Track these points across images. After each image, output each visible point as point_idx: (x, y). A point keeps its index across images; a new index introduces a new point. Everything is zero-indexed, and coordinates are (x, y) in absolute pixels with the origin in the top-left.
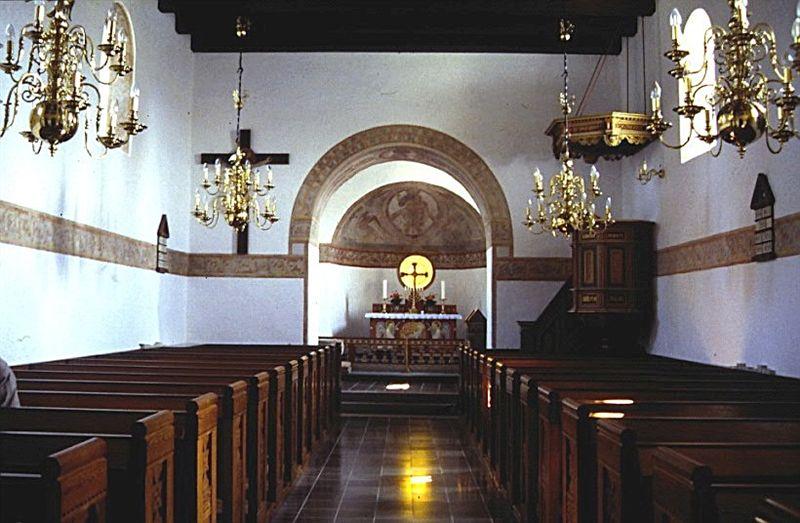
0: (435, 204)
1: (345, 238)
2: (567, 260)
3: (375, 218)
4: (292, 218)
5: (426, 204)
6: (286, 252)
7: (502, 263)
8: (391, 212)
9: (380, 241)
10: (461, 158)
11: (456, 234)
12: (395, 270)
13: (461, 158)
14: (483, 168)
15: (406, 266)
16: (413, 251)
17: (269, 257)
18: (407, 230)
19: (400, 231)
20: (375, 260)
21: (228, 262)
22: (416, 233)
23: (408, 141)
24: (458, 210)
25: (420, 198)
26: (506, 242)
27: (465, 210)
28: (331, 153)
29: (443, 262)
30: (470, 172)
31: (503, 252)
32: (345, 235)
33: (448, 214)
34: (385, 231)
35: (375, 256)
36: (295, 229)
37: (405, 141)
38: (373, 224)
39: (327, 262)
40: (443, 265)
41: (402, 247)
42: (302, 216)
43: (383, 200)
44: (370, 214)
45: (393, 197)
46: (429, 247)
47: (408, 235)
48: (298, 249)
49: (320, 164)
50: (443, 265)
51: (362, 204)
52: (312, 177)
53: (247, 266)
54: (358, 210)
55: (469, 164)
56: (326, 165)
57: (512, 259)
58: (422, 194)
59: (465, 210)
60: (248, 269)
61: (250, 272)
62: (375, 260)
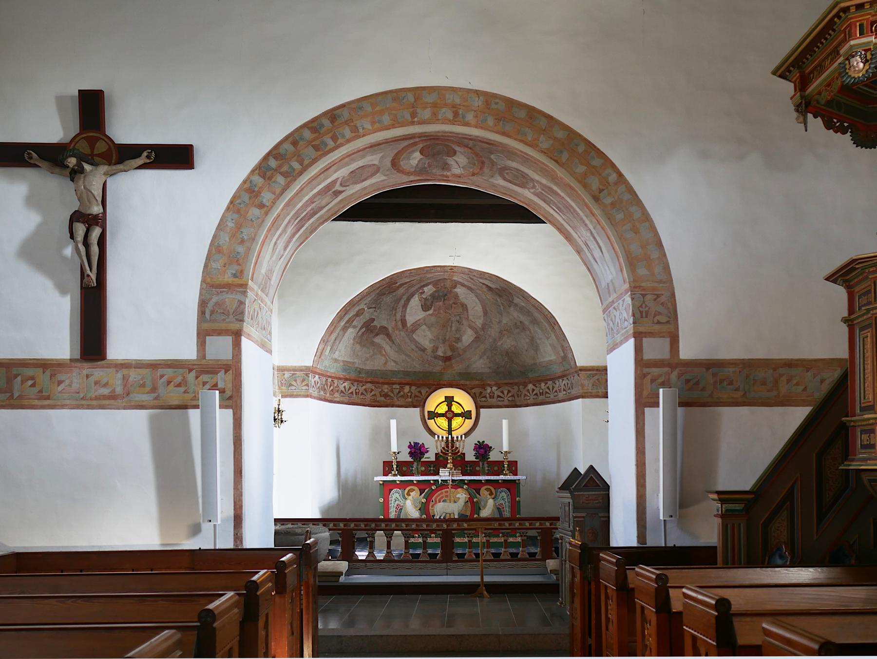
0: (479, 308)
1: (336, 360)
2: (679, 357)
3: (384, 330)
4: (204, 281)
5: (464, 307)
6: (188, 351)
7: (655, 371)
8: (410, 320)
9: (391, 366)
10: (565, 157)
11: (511, 355)
12: (418, 410)
13: (565, 157)
14: (613, 177)
15: (436, 401)
16: (447, 377)
17: (154, 365)
18: (435, 349)
19: (424, 350)
20: (386, 396)
21: (60, 377)
22: (449, 353)
23: (452, 122)
24: (516, 314)
25: (456, 296)
26: (665, 328)
27: (528, 313)
28: (288, 146)
29: (492, 397)
30: (585, 186)
31: (656, 349)
32: (336, 356)
33: (500, 322)
34: (400, 350)
35: (386, 389)
36: (210, 305)
37: (446, 121)
38: (379, 340)
39: (307, 396)
40: (494, 401)
41: (426, 374)
42: (228, 278)
43: (398, 301)
44: (375, 323)
45: (412, 295)
46: (469, 374)
47: (436, 357)
48: (219, 348)
49: (262, 169)
50: (494, 401)
51: (362, 306)
52: (246, 197)
53: (106, 385)
54: (358, 315)
55: (581, 169)
56: (276, 170)
57: (674, 363)
58: (459, 290)
59: (528, 313)
60: (105, 391)
61: (113, 397)
62: (386, 396)
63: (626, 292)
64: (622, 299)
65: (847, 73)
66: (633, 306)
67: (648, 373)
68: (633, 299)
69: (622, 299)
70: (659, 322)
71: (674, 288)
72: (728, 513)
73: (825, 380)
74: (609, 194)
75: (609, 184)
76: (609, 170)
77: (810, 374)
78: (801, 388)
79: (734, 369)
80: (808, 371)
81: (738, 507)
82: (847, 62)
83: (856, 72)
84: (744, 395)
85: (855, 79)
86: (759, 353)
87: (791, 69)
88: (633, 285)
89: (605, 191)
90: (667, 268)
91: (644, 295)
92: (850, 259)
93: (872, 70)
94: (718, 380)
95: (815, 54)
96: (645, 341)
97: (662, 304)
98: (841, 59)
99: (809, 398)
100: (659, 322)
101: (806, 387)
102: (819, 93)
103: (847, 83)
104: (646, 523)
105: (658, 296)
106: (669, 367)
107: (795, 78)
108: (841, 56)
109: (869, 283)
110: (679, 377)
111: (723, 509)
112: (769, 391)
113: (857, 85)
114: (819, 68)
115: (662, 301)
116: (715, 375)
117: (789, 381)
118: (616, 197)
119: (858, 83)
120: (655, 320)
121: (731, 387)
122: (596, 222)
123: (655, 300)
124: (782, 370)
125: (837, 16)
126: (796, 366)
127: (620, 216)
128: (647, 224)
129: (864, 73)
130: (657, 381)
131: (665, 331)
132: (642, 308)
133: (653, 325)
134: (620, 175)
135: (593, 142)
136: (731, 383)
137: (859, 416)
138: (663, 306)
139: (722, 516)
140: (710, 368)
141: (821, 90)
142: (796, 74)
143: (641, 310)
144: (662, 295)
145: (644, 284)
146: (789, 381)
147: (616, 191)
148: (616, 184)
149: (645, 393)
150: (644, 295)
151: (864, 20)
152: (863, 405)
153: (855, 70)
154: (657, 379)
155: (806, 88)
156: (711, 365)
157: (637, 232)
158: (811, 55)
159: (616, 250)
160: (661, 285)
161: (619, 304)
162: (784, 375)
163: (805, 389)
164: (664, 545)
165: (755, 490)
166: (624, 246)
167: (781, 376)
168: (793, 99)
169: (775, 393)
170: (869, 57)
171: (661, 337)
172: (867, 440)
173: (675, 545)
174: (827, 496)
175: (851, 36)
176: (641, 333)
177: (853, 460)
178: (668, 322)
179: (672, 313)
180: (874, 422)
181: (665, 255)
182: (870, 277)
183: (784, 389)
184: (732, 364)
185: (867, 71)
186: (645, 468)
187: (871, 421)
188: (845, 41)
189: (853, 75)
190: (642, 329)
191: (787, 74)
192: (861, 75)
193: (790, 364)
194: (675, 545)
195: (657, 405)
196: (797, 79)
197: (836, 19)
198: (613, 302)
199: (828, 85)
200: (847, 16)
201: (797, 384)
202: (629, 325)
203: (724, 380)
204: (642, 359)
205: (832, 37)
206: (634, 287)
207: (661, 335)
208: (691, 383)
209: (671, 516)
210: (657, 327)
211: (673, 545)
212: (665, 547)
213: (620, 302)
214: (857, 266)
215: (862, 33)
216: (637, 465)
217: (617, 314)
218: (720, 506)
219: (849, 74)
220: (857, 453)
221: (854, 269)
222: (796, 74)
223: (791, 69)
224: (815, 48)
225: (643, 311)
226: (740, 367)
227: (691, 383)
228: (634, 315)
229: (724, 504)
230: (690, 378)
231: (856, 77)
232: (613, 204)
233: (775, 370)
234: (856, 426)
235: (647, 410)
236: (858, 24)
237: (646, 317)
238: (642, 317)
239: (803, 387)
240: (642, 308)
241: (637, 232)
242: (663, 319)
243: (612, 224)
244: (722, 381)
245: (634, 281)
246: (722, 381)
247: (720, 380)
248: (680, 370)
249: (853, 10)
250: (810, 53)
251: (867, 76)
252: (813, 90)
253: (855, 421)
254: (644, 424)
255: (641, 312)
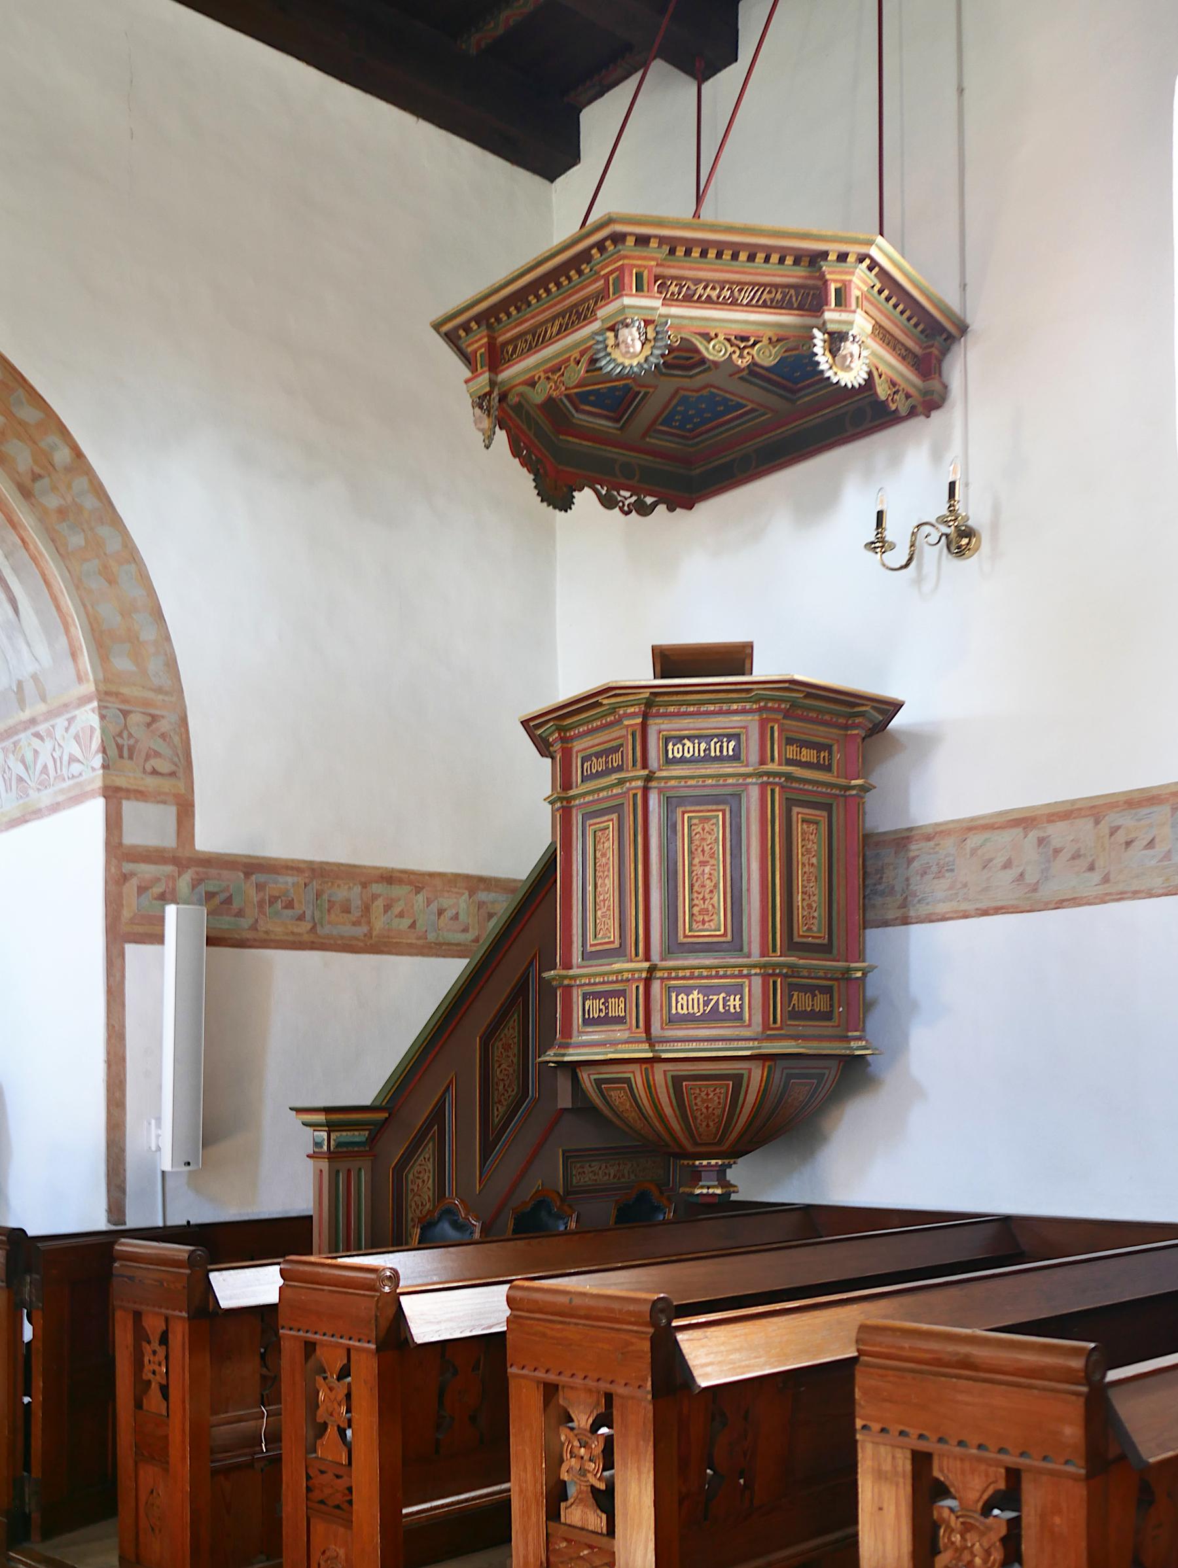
7: (147, 870)
14: (62, 456)
26: (166, 785)
63: (83, 701)
64: (68, 716)
65: (609, 354)
66: (104, 731)
67: (133, 874)
68: (102, 717)
69: (68, 716)
70: (155, 772)
71: (185, 707)
72: (340, 1150)
73: (445, 910)
74: (54, 488)
75: (53, 466)
76: (54, 439)
77: (421, 898)
78: (407, 922)
79: (295, 879)
80: (417, 893)
81: (360, 1136)
82: (611, 335)
83: (629, 355)
84: (313, 929)
85: (624, 367)
86: (337, 853)
87: (473, 325)
88: (103, 688)
89: (46, 481)
90: (171, 665)
91: (125, 714)
92: (604, 685)
93: (657, 359)
94: (267, 898)
95: (528, 310)
96: (129, 807)
97: (163, 736)
98: (596, 326)
99: (420, 942)
100: (155, 772)
101: (414, 922)
102: (532, 383)
103: (609, 372)
104: (124, 1181)
105: (154, 718)
106: (173, 864)
107: (476, 346)
108: (596, 319)
109: (624, 732)
110: (194, 887)
111: (332, 1142)
112: (354, 924)
113: (625, 379)
114: (529, 337)
115: (163, 730)
116: (260, 887)
117: (387, 908)
118: (69, 499)
119: (628, 377)
120: (148, 768)
121: (289, 912)
122: (19, 542)
123: (149, 725)
124: (376, 888)
125: (600, 246)
126: (401, 882)
127: (76, 540)
128: (133, 568)
129: (642, 361)
130: (150, 890)
131: (167, 790)
132: (122, 738)
133: (144, 776)
134: (78, 454)
135: (20, 370)
136: (290, 905)
137: (579, 967)
138: (164, 740)
139: (332, 1156)
140: (252, 874)
141: (536, 378)
142: (480, 339)
143: (119, 741)
144: (163, 717)
145: (125, 690)
146: (387, 908)
147: (69, 487)
148: (68, 470)
149: (126, 914)
150: (125, 714)
151: (645, 267)
152: (589, 949)
153: (628, 352)
154: (151, 888)
155: (501, 368)
156: (252, 867)
157: (112, 581)
158: (518, 309)
159: (64, 610)
160: (160, 697)
161: (53, 727)
162: (380, 895)
163: (413, 925)
164: (160, 1224)
165: (384, 1103)
166: (84, 606)
167: (375, 897)
168: (470, 384)
169: (364, 929)
170: (651, 335)
171: (158, 802)
172: (601, 1010)
173: (188, 1222)
174: (496, 1113)
175: (619, 290)
176: (118, 789)
177: (567, 1046)
178: (173, 774)
179: (181, 756)
180: (630, 976)
181: (168, 638)
182: (626, 723)
183: (380, 922)
184: (292, 868)
185: (646, 359)
186: (124, 1068)
187: (626, 975)
188: (602, 297)
189: (620, 360)
190: (121, 782)
191: (462, 333)
192: (635, 364)
193: (390, 877)
194: (188, 1222)
195: (159, 939)
196: (480, 347)
197: (594, 251)
198: (33, 721)
199: (556, 369)
200: (619, 251)
201: (401, 915)
202: (91, 769)
203: (277, 898)
204: (120, 844)
205: (572, 284)
206: (107, 693)
207: (159, 799)
208: (217, 901)
209: (189, 1164)
210: (151, 782)
211: (185, 1223)
212: (165, 1227)
213: (61, 722)
214: (605, 702)
215: (639, 288)
216: (109, 1063)
217: (45, 748)
218: (326, 1137)
219: (613, 356)
220: (575, 1032)
221: (598, 704)
222: (477, 343)
223: (473, 325)
224: (531, 298)
225: (123, 745)
226: (307, 875)
227: (217, 901)
228: (104, 751)
229: (334, 1131)
230: (215, 890)
231: (626, 364)
232: (62, 512)
233: (364, 885)
234: (572, 986)
235: (130, 949)
236: (634, 271)
237: (131, 757)
238: (121, 756)
239: (410, 921)
240: (122, 738)
241: (112, 581)
242: (164, 766)
243: (61, 555)
244: (273, 900)
245: (106, 680)
246: (273, 900)
247: (270, 897)
248: (197, 873)
249: (630, 241)
250: (519, 304)
251: (646, 366)
252: (518, 375)
253: (574, 978)
254: (123, 976)
255: (120, 748)
